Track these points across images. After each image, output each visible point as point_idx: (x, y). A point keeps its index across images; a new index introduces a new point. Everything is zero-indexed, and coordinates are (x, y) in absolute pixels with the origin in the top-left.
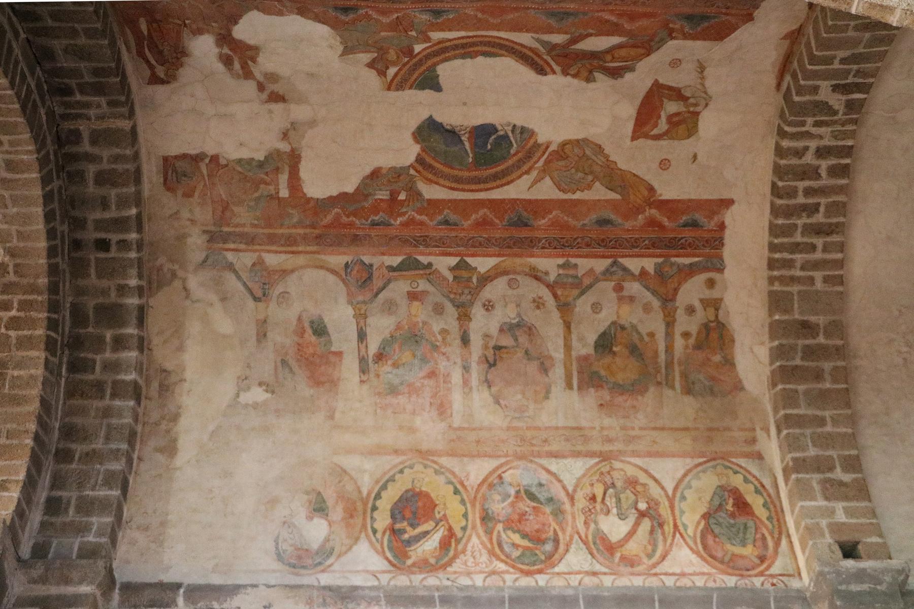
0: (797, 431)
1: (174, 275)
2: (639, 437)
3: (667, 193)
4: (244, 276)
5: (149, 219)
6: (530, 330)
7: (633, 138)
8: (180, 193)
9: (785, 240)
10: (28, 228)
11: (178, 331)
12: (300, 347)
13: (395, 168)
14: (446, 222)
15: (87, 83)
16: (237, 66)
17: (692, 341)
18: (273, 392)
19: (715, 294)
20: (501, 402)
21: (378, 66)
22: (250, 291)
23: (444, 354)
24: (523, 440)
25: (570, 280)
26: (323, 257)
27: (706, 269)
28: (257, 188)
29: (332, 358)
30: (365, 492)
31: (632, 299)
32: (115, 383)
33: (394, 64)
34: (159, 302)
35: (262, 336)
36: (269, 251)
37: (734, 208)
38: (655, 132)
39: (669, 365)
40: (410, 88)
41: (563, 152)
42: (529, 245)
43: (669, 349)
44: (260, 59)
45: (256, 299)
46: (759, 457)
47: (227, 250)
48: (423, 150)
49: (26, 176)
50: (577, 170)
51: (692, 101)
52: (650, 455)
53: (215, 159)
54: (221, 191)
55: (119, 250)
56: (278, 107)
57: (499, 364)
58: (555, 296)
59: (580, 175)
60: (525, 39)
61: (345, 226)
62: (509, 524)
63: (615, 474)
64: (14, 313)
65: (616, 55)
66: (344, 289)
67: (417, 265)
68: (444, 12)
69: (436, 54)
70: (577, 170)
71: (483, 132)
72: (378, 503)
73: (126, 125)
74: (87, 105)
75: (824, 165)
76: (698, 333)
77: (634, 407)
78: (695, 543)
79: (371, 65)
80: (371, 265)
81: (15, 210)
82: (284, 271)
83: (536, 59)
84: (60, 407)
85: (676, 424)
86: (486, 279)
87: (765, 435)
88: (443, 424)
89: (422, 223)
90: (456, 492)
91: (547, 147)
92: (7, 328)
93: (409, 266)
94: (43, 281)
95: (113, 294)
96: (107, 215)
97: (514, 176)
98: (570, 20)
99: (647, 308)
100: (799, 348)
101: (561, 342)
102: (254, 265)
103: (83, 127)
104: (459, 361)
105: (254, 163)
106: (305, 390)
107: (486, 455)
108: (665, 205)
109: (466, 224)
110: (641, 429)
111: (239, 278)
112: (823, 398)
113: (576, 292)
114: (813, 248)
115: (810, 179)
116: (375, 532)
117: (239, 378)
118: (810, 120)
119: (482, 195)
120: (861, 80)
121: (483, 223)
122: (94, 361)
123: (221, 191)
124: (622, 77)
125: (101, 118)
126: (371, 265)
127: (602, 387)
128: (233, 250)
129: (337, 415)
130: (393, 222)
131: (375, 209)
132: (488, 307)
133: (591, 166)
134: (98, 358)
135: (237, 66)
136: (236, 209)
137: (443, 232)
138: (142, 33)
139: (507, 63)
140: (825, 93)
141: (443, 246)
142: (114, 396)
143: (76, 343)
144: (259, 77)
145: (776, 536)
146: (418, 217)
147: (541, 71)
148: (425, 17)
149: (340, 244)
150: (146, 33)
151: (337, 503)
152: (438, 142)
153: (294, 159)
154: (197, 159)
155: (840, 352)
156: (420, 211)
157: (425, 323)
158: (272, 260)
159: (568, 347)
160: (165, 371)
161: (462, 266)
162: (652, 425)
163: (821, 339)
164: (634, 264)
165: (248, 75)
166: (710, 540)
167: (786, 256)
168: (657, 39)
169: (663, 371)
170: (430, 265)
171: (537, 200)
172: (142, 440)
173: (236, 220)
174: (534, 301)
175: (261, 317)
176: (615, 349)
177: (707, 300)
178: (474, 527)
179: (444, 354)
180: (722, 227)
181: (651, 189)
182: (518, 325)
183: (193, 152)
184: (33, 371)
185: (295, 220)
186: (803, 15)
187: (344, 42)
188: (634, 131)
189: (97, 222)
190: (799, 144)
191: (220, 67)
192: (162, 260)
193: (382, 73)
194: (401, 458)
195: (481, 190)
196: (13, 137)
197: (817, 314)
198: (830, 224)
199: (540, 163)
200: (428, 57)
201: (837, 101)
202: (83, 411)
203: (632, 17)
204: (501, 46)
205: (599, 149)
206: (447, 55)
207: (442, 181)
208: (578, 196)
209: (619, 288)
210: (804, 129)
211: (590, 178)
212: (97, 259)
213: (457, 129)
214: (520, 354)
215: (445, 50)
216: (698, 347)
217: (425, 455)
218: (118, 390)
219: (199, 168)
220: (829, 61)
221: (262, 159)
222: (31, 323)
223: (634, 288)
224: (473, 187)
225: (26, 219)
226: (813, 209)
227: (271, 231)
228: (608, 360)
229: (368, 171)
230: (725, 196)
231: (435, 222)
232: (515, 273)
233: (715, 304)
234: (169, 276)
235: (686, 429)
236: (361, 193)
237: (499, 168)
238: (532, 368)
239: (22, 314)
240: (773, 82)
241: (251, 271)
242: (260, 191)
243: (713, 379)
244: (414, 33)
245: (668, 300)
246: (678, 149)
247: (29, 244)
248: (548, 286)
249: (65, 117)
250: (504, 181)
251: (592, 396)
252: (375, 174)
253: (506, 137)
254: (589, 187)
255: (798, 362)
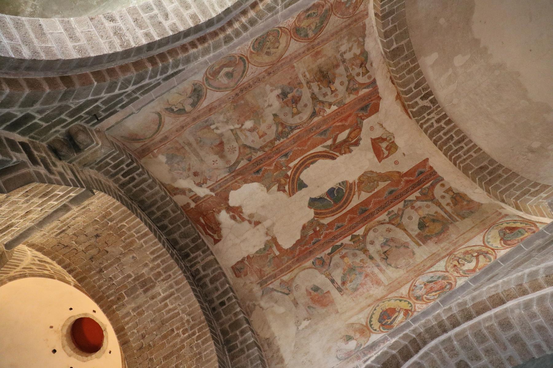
0: (508, 193)
1: (255, 305)
2: (458, 241)
3: (405, 170)
4: (279, 289)
5: (237, 291)
6: (392, 240)
7: (380, 162)
8: (243, 276)
9: (452, 151)
10: (190, 302)
11: (265, 322)
12: (312, 299)
13: (309, 221)
14: (338, 227)
15: (193, 247)
16: (238, 218)
17: (452, 205)
18: (311, 319)
19: (447, 187)
20: (398, 267)
21: (281, 189)
22: (284, 293)
23: (366, 267)
24: (415, 271)
25: (394, 216)
26: (303, 265)
27: (437, 183)
28: (267, 258)
29: (326, 295)
30: (364, 324)
31: (420, 207)
32: (247, 346)
33: (285, 184)
34: (254, 318)
35: (296, 304)
36: (283, 276)
37: (430, 160)
38: (385, 155)
39: (450, 216)
40: (297, 191)
41: (361, 181)
42: (372, 216)
43: (446, 212)
44: (244, 211)
45: (287, 294)
46: (506, 215)
47: (269, 285)
48: (315, 209)
49: (183, 284)
50: (370, 183)
51: (388, 139)
52: (466, 242)
53: (248, 257)
54: (256, 266)
55: (229, 302)
56: (259, 226)
57: (389, 257)
58: (393, 224)
59: (372, 184)
60: (319, 149)
61: (304, 251)
62: (427, 293)
63: (458, 255)
64: (197, 334)
65: (352, 137)
66: (317, 271)
67: (338, 247)
68: (288, 153)
69: (296, 172)
70: (370, 183)
71: (331, 192)
72: (372, 323)
73: (211, 257)
74: (196, 257)
75: (442, 123)
76: (452, 201)
77: (448, 235)
78: (504, 247)
79: (279, 190)
80: (322, 257)
81: (184, 298)
82: (292, 279)
83: (329, 154)
84: (230, 365)
85: (468, 229)
86: (365, 235)
87: (503, 209)
88: (381, 287)
89: (330, 233)
90: (400, 301)
91: (355, 183)
92: (197, 341)
93: (335, 249)
94: (203, 317)
95: (233, 318)
96: (219, 292)
97: (350, 198)
98: (328, 133)
99: (428, 206)
100: (486, 175)
101: (406, 236)
102: (280, 284)
103: (199, 267)
104: (374, 265)
105: (262, 250)
106: (323, 311)
107: (404, 284)
108: (406, 174)
109: (346, 223)
110: (456, 239)
111: (278, 291)
112: (507, 180)
113: (399, 218)
114: (462, 147)
115: (442, 130)
116: (375, 330)
117: (295, 323)
118: (425, 115)
119: (345, 211)
120: (427, 92)
121: (351, 220)
122: (236, 344)
123: (256, 266)
124: (360, 144)
125: (203, 260)
126: (322, 257)
127: (432, 238)
128: (270, 283)
129: (339, 310)
130: (320, 239)
131: (311, 238)
132: (372, 243)
133: (373, 179)
134: (237, 342)
135: (238, 218)
136: (264, 269)
137: (339, 231)
138: (203, 223)
139: (321, 162)
140: (422, 103)
141: (343, 235)
142: (248, 350)
143: (227, 342)
144: (247, 218)
145: (533, 225)
146: (327, 232)
147: (333, 158)
148: (283, 159)
149: (306, 258)
150: (204, 223)
151: (355, 333)
152: (319, 204)
153: (274, 240)
154: (242, 261)
155: (500, 166)
156: (327, 229)
157: (353, 262)
158: (286, 278)
159: (410, 236)
160: (267, 339)
161: (353, 237)
162: (460, 235)
163: (491, 168)
164: (412, 197)
165: (243, 219)
166: (509, 242)
167: (456, 155)
168: (359, 123)
169: (450, 219)
170: (342, 244)
171: (364, 201)
172: (268, 363)
173: (266, 273)
174: (387, 231)
175: (293, 299)
176: (427, 225)
177: (446, 190)
178: (415, 303)
179: (366, 267)
180: (431, 168)
181: (398, 172)
182: (387, 241)
183: (240, 259)
184: (211, 349)
185: (286, 259)
186: (394, 88)
187: (265, 186)
188: (378, 160)
189: (217, 297)
190: (429, 123)
191: (233, 222)
192: (248, 303)
193: (284, 191)
194: (372, 306)
195: (343, 210)
196: (173, 271)
197: (482, 162)
198: (461, 138)
199: (356, 189)
200: (294, 175)
201: (426, 103)
202: (239, 362)
203: (345, 119)
204: (314, 157)
205: (372, 172)
206: (300, 170)
207: (328, 215)
208: (376, 190)
209: (413, 207)
210: (426, 119)
211: (376, 182)
212: (222, 310)
213: (322, 196)
214: (394, 249)
215: (298, 169)
216: (455, 204)
217: (381, 299)
218: (249, 347)
219: (245, 263)
220: (410, 91)
221: (264, 247)
222: (205, 334)
223: (418, 203)
224: (340, 211)
225: (189, 299)
226: (452, 137)
227: (281, 268)
228: (427, 230)
229: (301, 228)
230: (424, 158)
231: (334, 230)
232: (373, 227)
233: (450, 189)
234: (253, 306)
235: (473, 227)
236: (303, 237)
237: (344, 199)
238: (402, 249)
239: (200, 333)
240: (407, 117)
241: (280, 286)
242: (269, 258)
243: (469, 209)
244: (284, 168)
245: (433, 199)
246: (397, 155)
247: (193, 308)
248: (388, 223)
249: (192, 266)
250: (348, 202)
251: (430, 243)
252: (304, 227)
253: (339, 188)
254: (378, 185)
255: (489, 178)
